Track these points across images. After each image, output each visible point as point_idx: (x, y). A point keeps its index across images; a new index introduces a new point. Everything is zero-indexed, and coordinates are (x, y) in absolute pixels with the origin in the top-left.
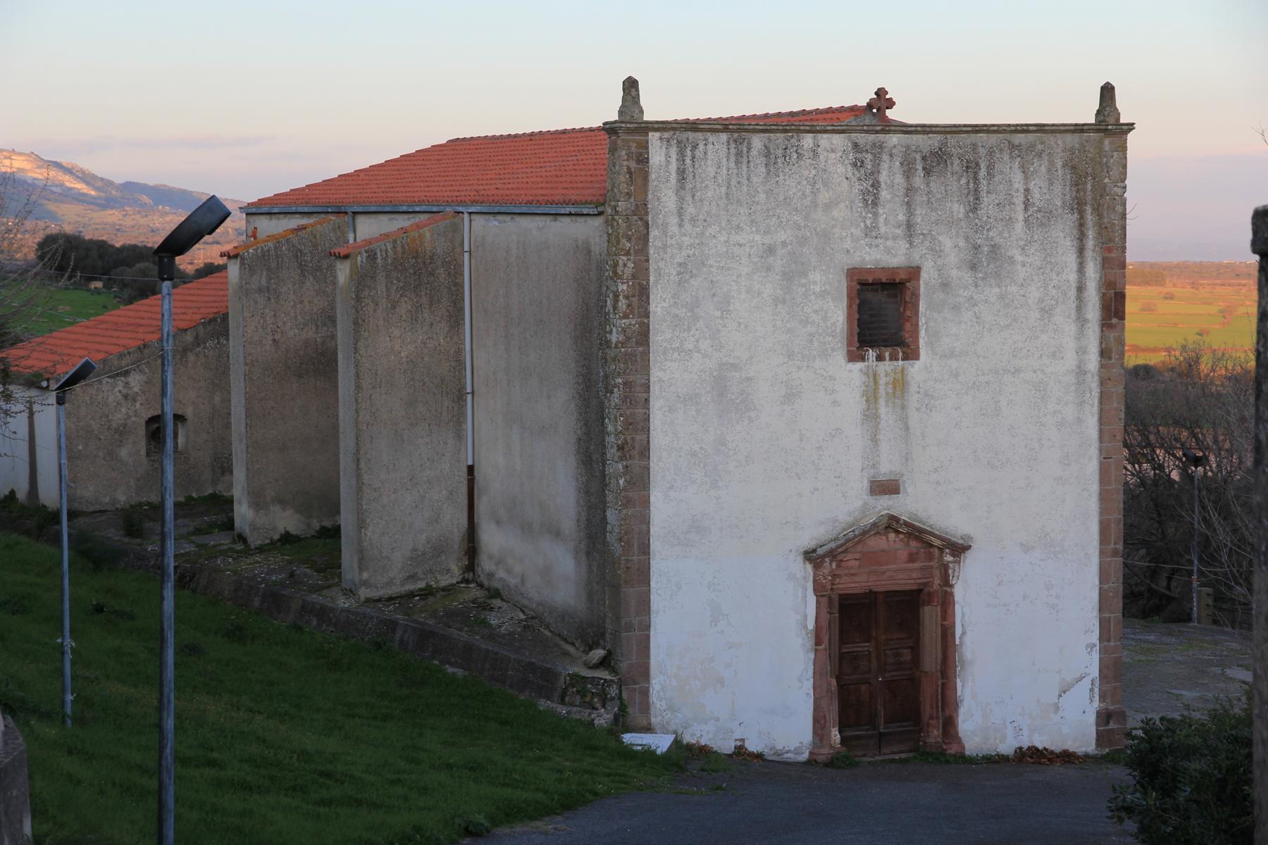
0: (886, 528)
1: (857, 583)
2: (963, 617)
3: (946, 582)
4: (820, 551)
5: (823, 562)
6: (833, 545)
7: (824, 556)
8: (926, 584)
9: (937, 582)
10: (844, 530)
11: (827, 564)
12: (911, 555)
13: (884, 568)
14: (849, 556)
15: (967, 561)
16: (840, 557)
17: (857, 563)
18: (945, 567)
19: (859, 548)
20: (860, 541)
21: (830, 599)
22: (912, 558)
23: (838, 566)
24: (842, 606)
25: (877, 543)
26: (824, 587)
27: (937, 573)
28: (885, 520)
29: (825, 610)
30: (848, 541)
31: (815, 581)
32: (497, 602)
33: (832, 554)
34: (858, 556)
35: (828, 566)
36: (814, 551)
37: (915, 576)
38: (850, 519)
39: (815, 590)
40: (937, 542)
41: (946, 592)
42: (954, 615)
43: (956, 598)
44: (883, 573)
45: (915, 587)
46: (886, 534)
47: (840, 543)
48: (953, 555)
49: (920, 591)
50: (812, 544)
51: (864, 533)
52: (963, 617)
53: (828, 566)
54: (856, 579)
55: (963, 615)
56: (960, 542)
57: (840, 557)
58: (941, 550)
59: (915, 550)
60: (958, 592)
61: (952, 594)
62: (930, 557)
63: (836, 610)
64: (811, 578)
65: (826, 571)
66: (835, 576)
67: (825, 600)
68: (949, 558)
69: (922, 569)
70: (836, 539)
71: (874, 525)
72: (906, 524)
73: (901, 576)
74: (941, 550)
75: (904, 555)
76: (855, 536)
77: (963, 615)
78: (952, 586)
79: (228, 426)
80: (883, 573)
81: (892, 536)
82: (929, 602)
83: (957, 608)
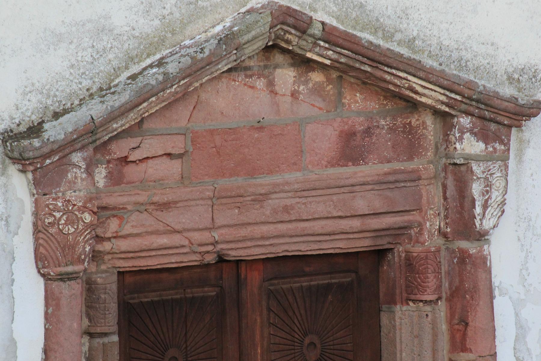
0: (268, 49)
1: (177, 228)
2: (520, 338)
3: (464, 225)
4: (55, 131)
5: (64, 163)
6: (96, 109)
7: (69, 145)
8: (399, 232)
9: (434, 223)
10: (131, 59)
11: (77, 173)
12: (348, 136)
13: (264, 181)
14: (151, 146)
15: (529, 153)
16: (119, 149)
17: (175, 166)
18: (459, 174)
19: (182, 117)
20: (184, 95)
21: (90, 288)
22: (351, 148)
23: (115, 179)
24: (132, 316)
25: (238, 102)
26: (68, 248)
27: (432, 194)
28: (263, 26)
29: (73, 321)
30: (143, 96)
31: (38, 229)
32: (95, 210)
33: (95, 140)
34: (177, 145)
35: (83, 181)
36: (35, 130)
37: (361, 204)
38: (148, 26)
39: (41, 259)
40: (431, 96)
41: (464, 258)
42: (491, 332)
43: (130, 75)
44: (261, 198)
45: (363, 244)
46: (266, 72)
47: (116, 101)
48: (484, 137)
49: (379, 255)
50: (28, 110)
51: (196, 69)
52: (520, 338)
53: (83, 181)
54: (172, 218)
55: (522, 330)
56: (507, 91)
57: (119, 149)
58: (444, 118)
59: (360, 123)
60: (507, 256)
61: (482, 263)
62: (410, 144)
63: (110, 320)
64: (28, 220)
65: (77, 196)
66: (103, 211)
67: (71, 292)
68: (470, 146)
69: (382, 183)
70: (104, 91)
71: (228, 39)
72: (331, 37)
73: (321, 209)
74: (444, 118)
75: (324, 138)
76: (168, 80)
77: (522, 330)
78: (481, 236)
79: (270, 172)
80: (261, 198)
81: (286, 76)
82: (411, 293)
83: (501, 305)
